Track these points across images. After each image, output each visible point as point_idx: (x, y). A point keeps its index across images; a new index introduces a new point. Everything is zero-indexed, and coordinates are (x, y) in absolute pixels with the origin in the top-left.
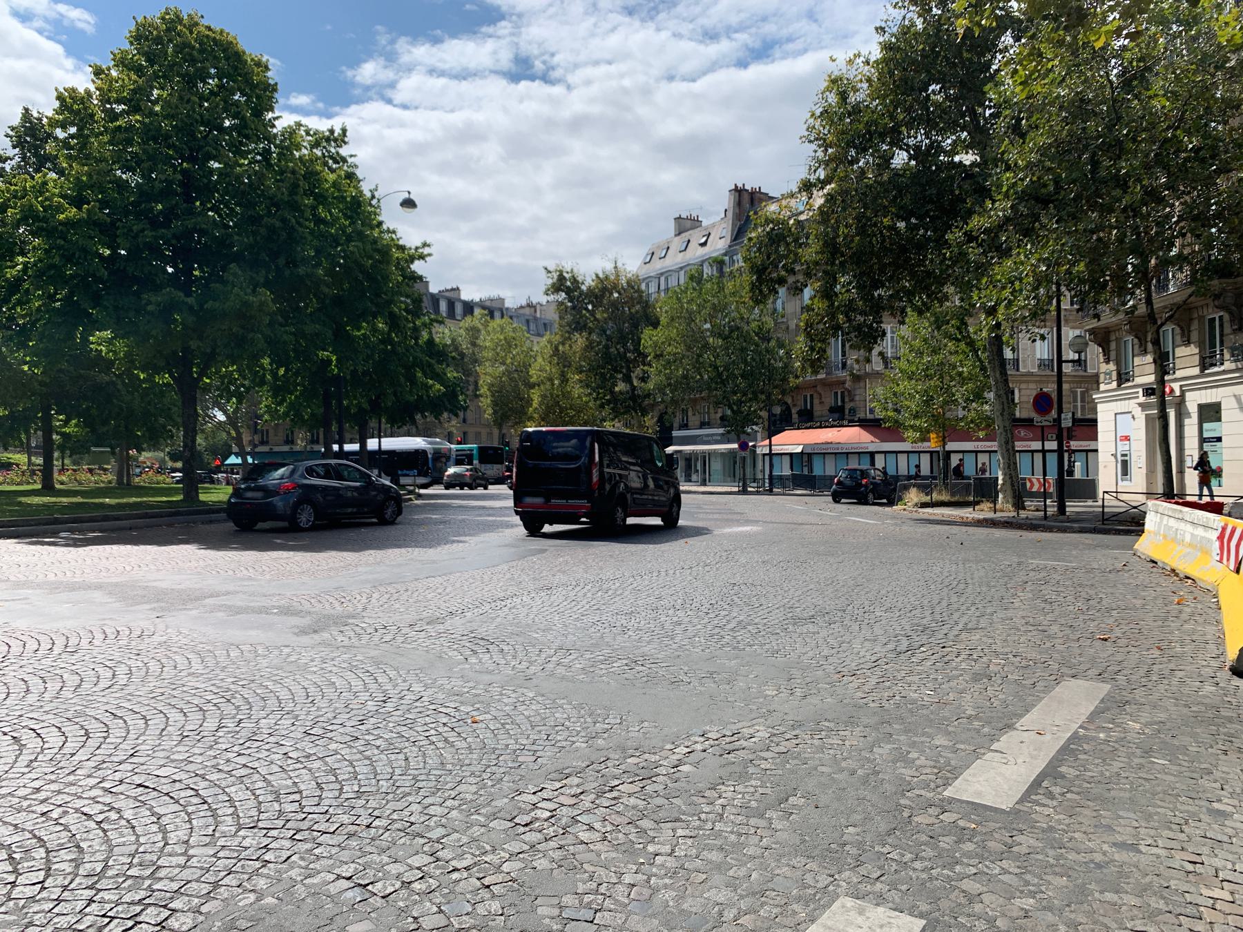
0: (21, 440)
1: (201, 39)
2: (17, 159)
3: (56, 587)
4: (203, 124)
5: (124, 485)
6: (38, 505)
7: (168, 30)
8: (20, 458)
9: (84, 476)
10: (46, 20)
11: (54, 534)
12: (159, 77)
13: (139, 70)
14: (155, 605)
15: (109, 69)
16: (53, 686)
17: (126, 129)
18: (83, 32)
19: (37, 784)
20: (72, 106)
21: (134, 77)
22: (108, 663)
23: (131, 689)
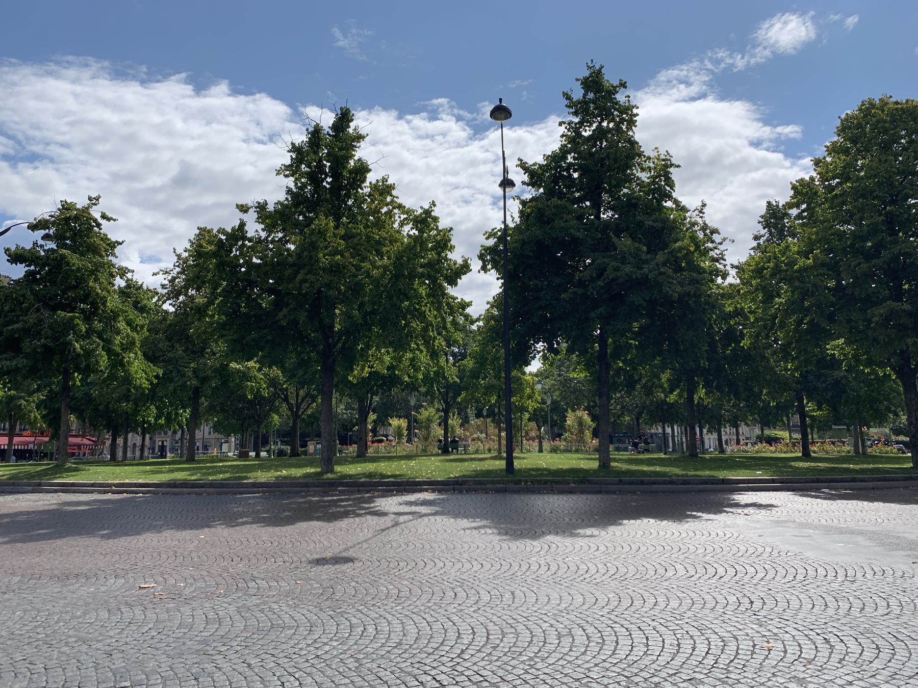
0: (783, 422)
1: (892, 114)
2: (767, 235)
3: (828, 530)
4: (898, 174)
5: (860, 455)
6: (803, 468)
7: (865, 116)
8: (784, 434)
9: (829, 447)
10: (771, 141)
11: (818, 490)
12: (862, 151)
13: (846, 151)
14: (909, 553)
15: (824, 158)
16: (844, 606)
17: (841, 195)
18: (794, 139)
19: (850, 678)
20: (803, 191)
21: (843, 158)
22: (881, 594)
23: (904, 619)
